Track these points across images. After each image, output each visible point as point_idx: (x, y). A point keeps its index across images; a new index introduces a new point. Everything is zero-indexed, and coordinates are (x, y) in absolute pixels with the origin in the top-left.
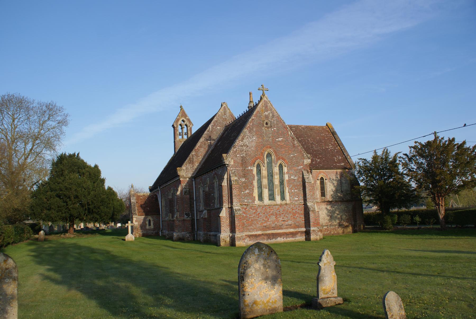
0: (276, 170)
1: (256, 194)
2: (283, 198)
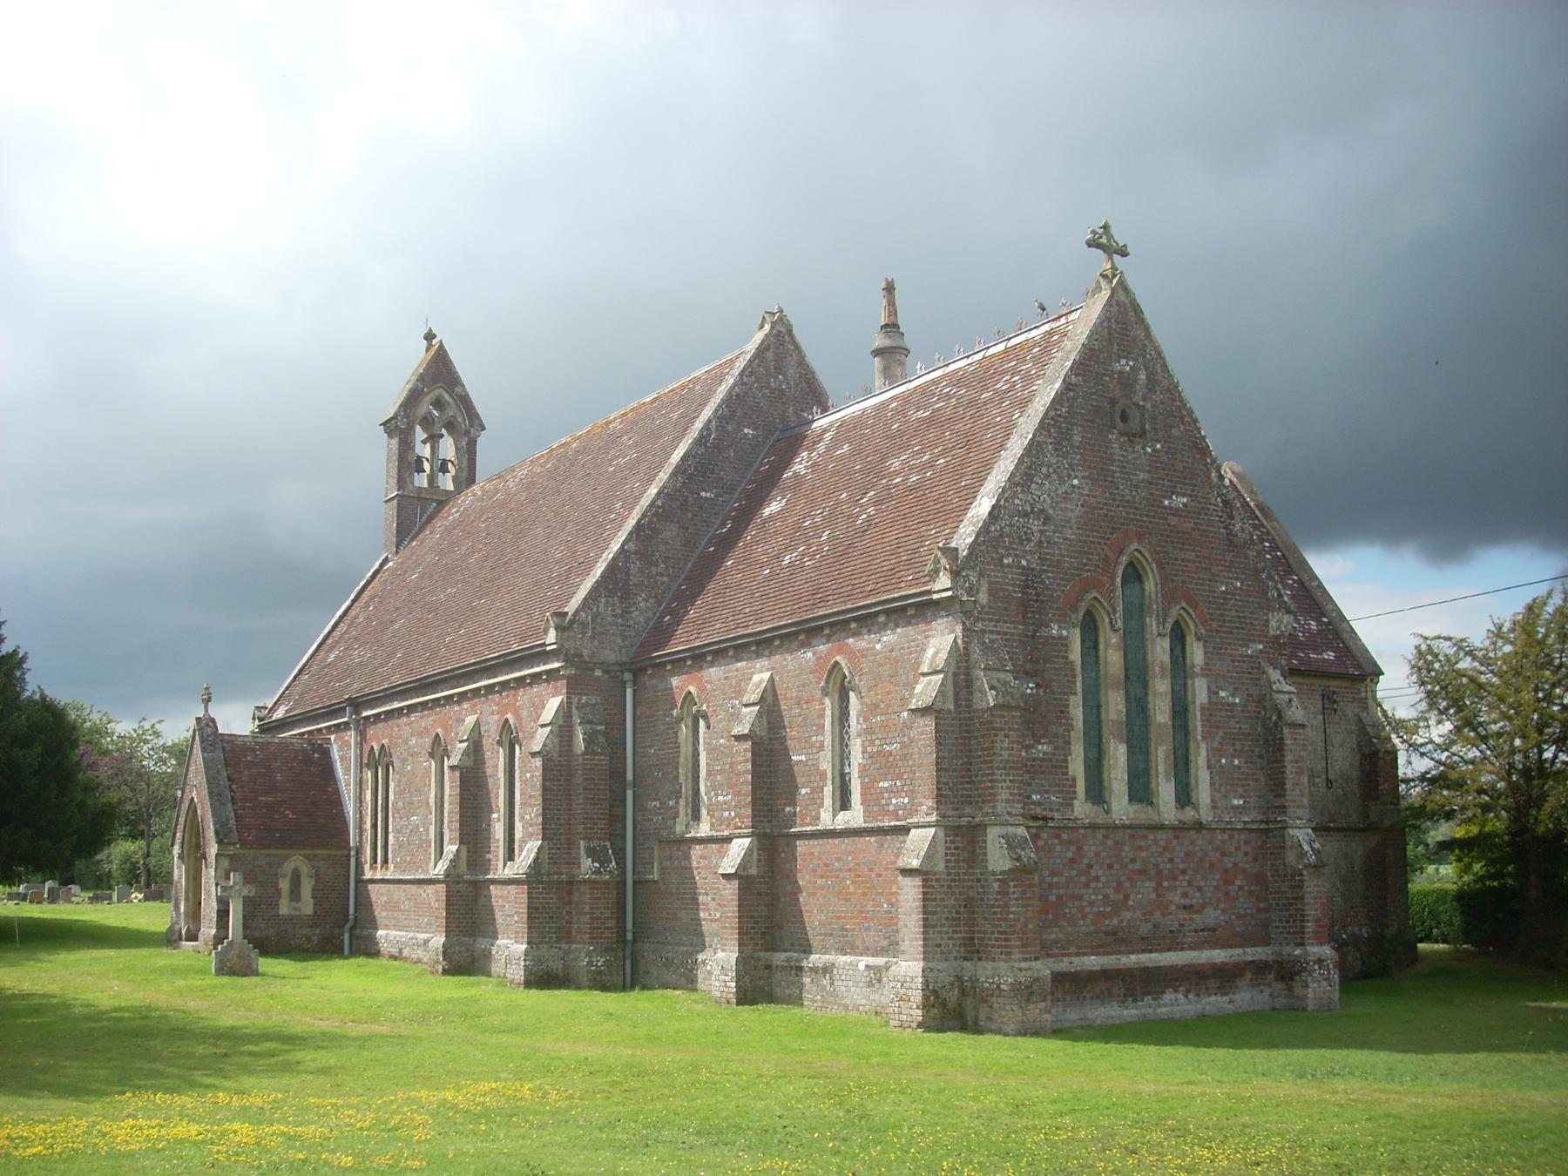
0: (1160, 650)
1: (1077, 766)
2: (1184, 797)
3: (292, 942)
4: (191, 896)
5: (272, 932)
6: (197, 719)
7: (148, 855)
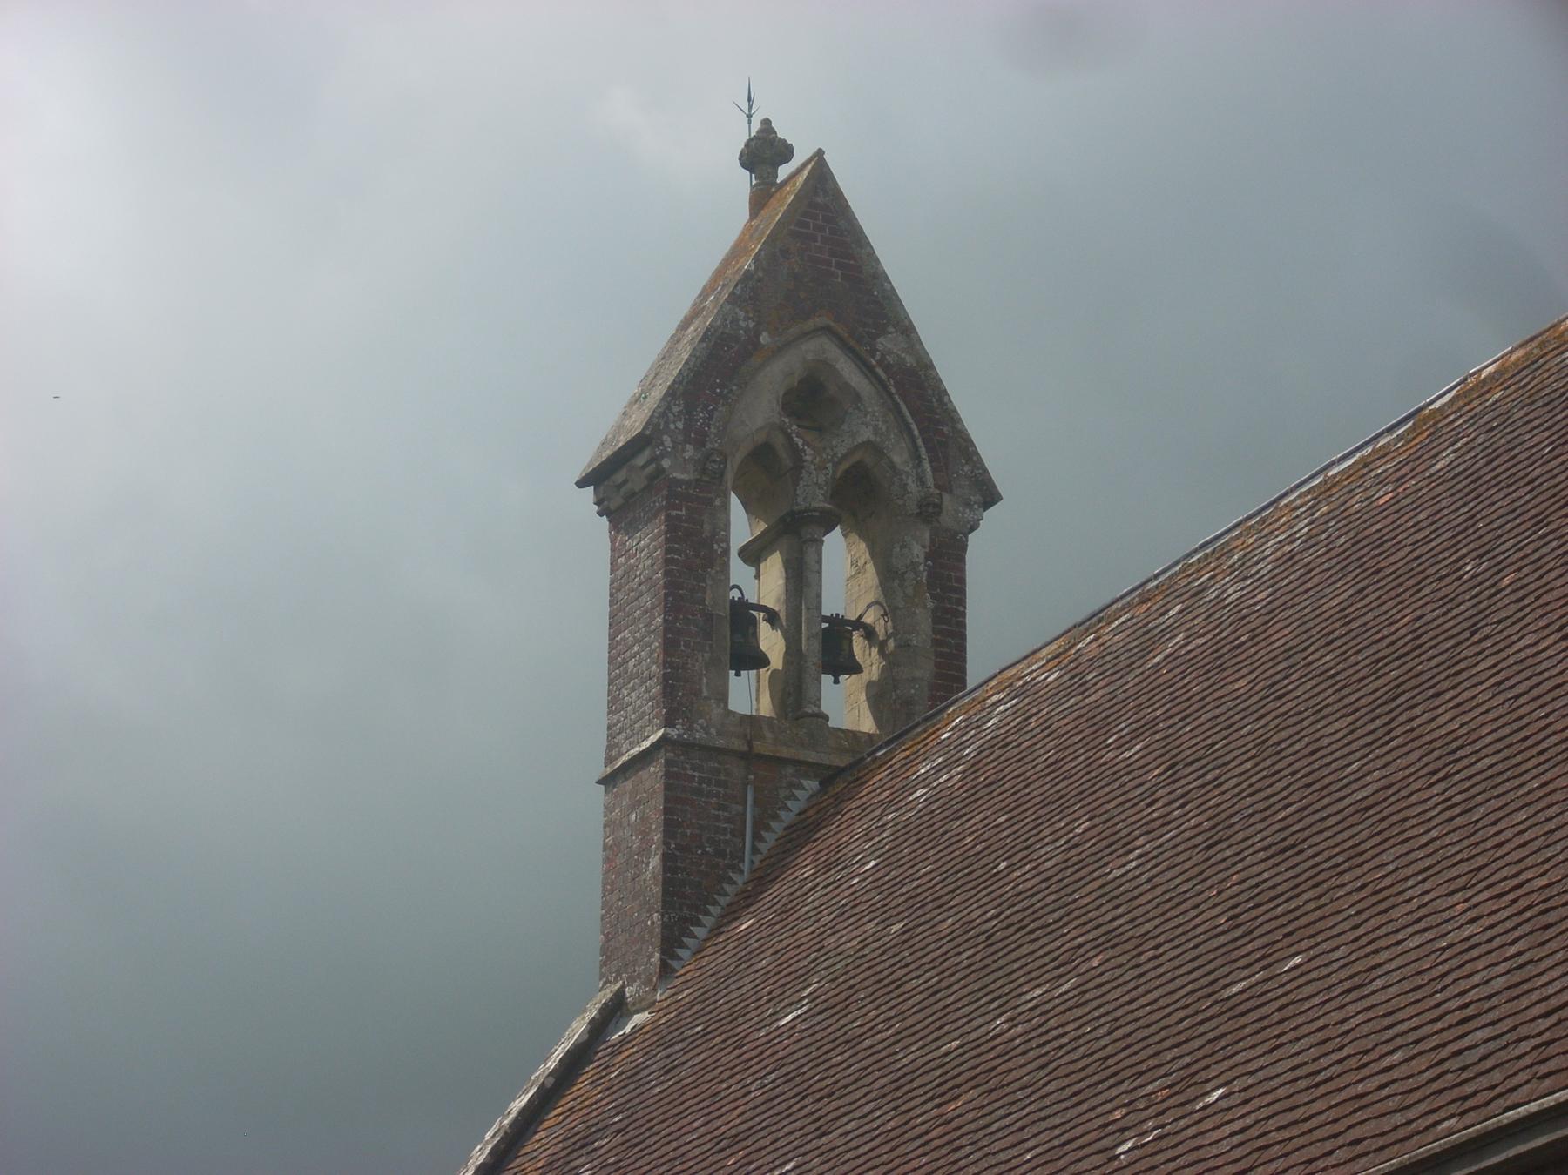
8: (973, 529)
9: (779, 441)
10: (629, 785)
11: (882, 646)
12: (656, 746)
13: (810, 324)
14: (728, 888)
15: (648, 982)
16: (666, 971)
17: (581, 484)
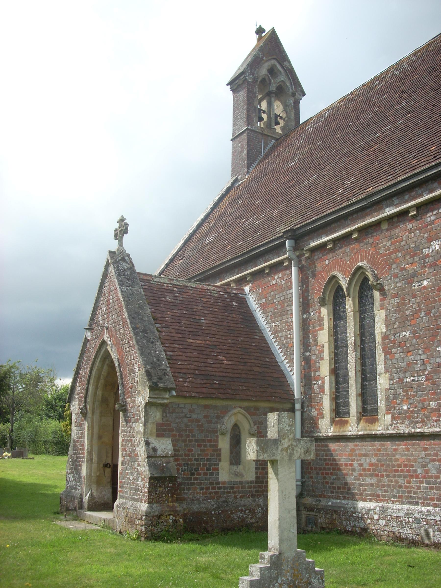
3: (235, 517)
4: (95, 457)
5: (211, 504)
6: (110, 252)
7: (12, 431)
8: (301, 99)
9: (267, 78)
10: (238, 139)
11: (284, 120)
12: (245, 130)
13: (273, 57)
14: (259, 158)
15: (244, 174)
16: (248, 172)
17: (227, 85)
